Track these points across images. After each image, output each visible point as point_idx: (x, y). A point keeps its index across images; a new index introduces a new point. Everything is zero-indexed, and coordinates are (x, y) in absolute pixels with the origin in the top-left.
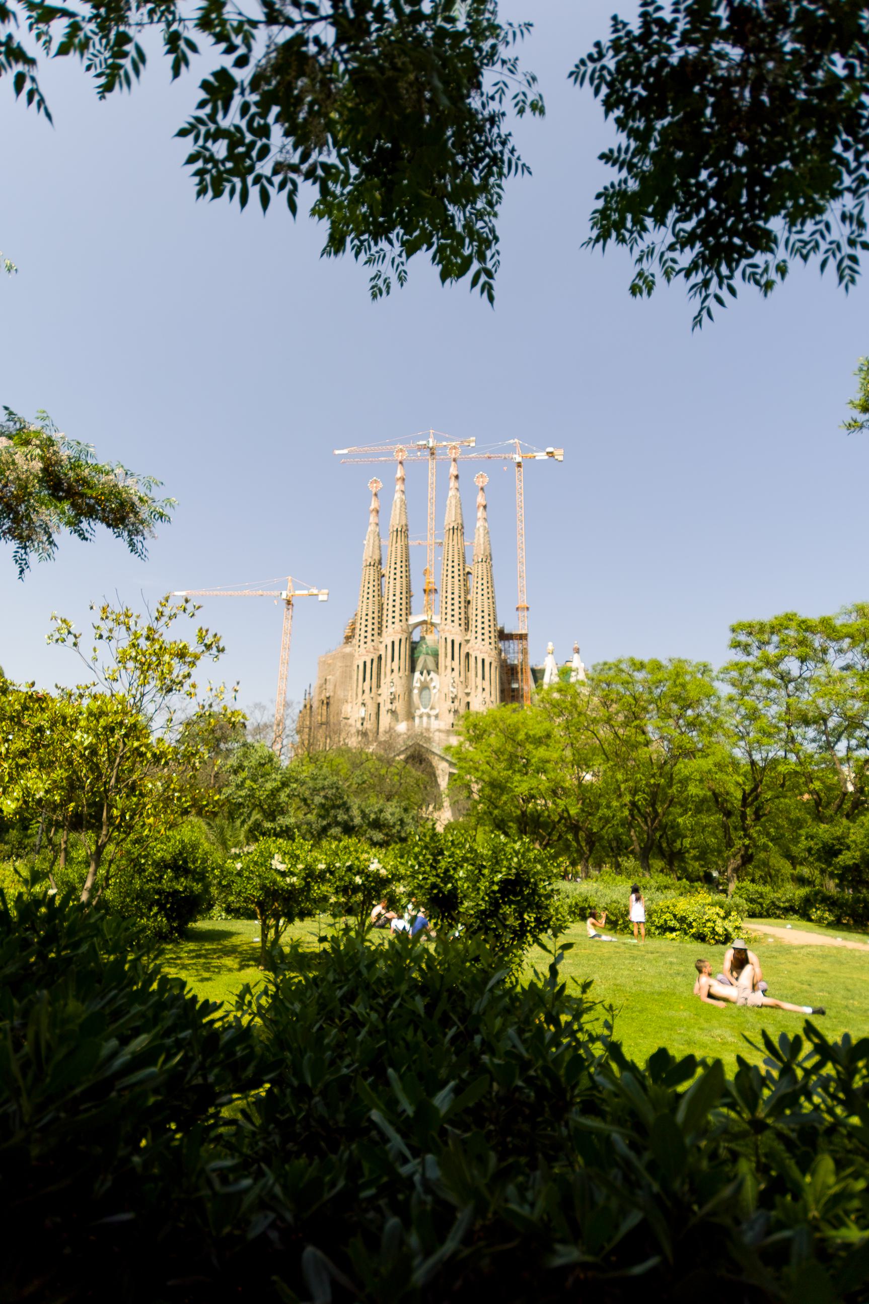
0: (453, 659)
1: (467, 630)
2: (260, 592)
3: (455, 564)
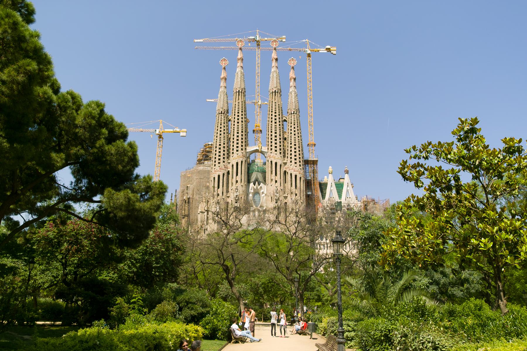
0: (276, 175)
1: (284, 156)
2: (141, 130)
3: (277, 114)
